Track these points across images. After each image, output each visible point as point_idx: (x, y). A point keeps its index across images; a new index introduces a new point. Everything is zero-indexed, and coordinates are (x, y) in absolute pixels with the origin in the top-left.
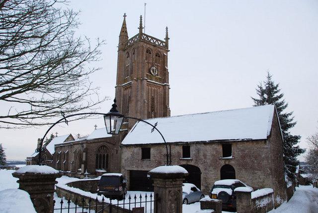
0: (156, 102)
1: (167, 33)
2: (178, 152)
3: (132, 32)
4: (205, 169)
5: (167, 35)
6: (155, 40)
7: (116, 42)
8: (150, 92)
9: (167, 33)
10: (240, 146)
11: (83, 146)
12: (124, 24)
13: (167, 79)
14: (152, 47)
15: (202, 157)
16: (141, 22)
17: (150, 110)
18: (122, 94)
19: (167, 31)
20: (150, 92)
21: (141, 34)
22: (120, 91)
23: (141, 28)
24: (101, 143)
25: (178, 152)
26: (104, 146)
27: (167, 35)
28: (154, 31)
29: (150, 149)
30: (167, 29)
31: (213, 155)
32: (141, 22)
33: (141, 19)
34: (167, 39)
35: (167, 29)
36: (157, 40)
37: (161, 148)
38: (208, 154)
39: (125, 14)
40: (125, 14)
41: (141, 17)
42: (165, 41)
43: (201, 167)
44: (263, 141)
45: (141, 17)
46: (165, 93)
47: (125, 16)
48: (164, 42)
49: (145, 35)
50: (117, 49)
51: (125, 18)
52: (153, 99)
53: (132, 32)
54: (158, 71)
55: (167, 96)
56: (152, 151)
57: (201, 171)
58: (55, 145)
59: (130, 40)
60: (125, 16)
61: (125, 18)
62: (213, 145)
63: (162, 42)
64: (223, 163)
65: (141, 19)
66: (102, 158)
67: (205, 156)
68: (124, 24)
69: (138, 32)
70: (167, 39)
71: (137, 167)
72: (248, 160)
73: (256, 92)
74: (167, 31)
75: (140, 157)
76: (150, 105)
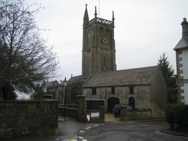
0: (106, 60)
1: (113, 15)
2: (109, 91)
3: (91, 17)
4: (122, 99)
5: (113, 16)
6: (105, 21)
7: (82, 22)
8: (103, 54)
9: (113, 15)
10: (138, 87)
11: (63, 88)
12: (86, 11)
13: (113, 46)
14: (103, 26)
15: (120, 93)
16: (96, 10)
17: (103, 66)
18: (86, 55)
19: (113, 14)
20: (103, 54)
21: (96, 18)
22: (85, 53)
23: (96, 14)
24: (124, 129)
25: (109, 91)
26: (76, 88)
27: (113, 16)
28: (105, 15)
29: (96, 89)
30: (113, 12)
31: (126, 92)
32: (96, 10)
33: (96, 9)
34: (113, 19)
35: (113, 12)
36: (107, 21)
37: (101, 89)
38: (123, 91)
39: (86, 4)
40: (86, 4)
41: (96, 7)
42: (112, 20)
43: (120, 98)
44: (148, 85)
45: (96, 7)
46: (112, 54)
47: (86, 5)
48: (111, 22)
49: (99, 18)
50: (82, 27)
51: (86, 7)
52: (105, 58)
53: (91, 17)
54: (107, 41)
55: (113, 56)
56: (97, 90)
57: (120, 100)
58: (182, 73)
59: (90, 21)
60: (86, 5)
61: (86, 7)
62: (125, 87)
63: (110, 21)
64: (130, 96)
65: (96, 9)
66: (73, 98)
67: (122, 92)
68: (86, 11)
69: (94, 17)
70: (113, 19)
71: (90, 98)
72: (141, 95)
73: (162, 53)
74: (113, 14)
75: (91, 93)
76: (103, 63)
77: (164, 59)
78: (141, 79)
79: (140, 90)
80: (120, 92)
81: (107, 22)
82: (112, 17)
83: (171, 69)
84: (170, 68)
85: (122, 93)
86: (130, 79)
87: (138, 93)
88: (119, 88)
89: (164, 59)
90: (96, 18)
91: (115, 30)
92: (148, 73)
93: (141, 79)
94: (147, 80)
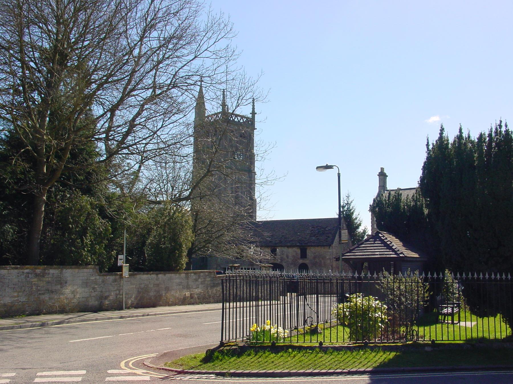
5: (253, 109)
6: (239, 118)
21: (225, 112)
27: (253, 109)
42: (250, 116)
64: (301, 261)
67: (287, 256)
70: (253, 113)
72: (317, 260)
77: (348, 203)
78: (317, 236)
79: (317, 254)
80: (285, 257)
81: (238, 119)
82: (439, 136)
83: (358, 219)
84: (356, 219)
85: (288, 258)
86: (299, 235)
87: (315, 258)
88: (283, 249)
89: (348, 203)
90: (225, 112)
91: (258, 137)
92: (149, 32)
93: (317, 236)
94: (327, 239)
